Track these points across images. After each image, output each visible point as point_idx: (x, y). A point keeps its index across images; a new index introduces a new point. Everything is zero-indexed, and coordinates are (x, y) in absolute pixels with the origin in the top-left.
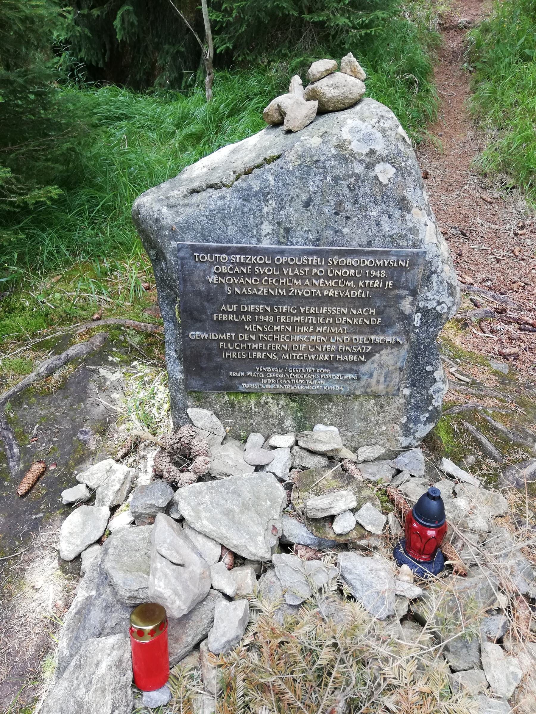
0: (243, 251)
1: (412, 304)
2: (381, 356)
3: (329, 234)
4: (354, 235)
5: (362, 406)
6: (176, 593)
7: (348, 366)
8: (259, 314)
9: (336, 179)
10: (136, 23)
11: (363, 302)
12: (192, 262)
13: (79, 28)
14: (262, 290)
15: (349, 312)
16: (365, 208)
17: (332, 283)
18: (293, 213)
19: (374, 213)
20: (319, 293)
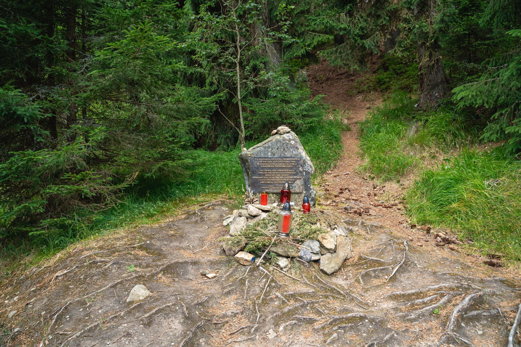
0: (265, 158)
3: (283, 155)
4: (288, 154)
11: (291, 168)
14: (269, 166)
18: (275, 150)
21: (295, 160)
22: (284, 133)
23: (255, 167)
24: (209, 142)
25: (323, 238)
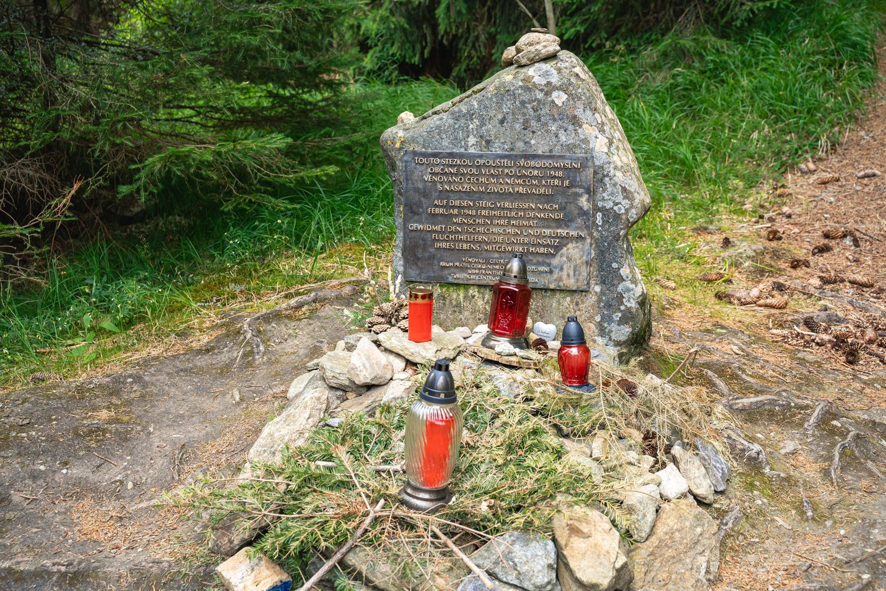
0: (451, 155)
1: (588, 201)
2: (568, 249)
3: (520, 145)
4: (539, 144)
5: (559, 302)
6: (364, 367)
7: (541, 259)
8: (464, 208)
9: (523, 103)
10: (464, 11)
12: (413, 165)
13: (394, 19)
15: (536, 206)
16: (546, 124)
17: (520, 181)
18: (491, 128)
19: (553, 128)
20: (511, 190)
21: (565, 168)
22: (532, 62)
23: (417, 190)
24: (470, 57)
25: (574, 531)
